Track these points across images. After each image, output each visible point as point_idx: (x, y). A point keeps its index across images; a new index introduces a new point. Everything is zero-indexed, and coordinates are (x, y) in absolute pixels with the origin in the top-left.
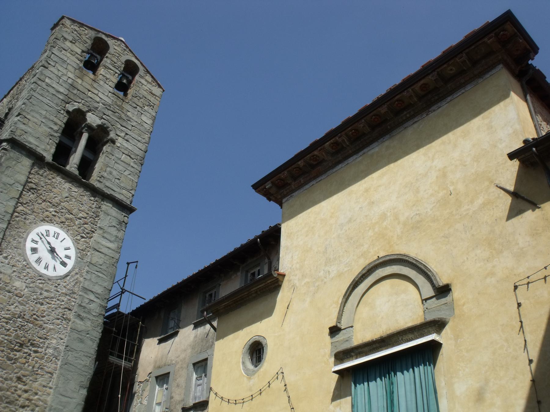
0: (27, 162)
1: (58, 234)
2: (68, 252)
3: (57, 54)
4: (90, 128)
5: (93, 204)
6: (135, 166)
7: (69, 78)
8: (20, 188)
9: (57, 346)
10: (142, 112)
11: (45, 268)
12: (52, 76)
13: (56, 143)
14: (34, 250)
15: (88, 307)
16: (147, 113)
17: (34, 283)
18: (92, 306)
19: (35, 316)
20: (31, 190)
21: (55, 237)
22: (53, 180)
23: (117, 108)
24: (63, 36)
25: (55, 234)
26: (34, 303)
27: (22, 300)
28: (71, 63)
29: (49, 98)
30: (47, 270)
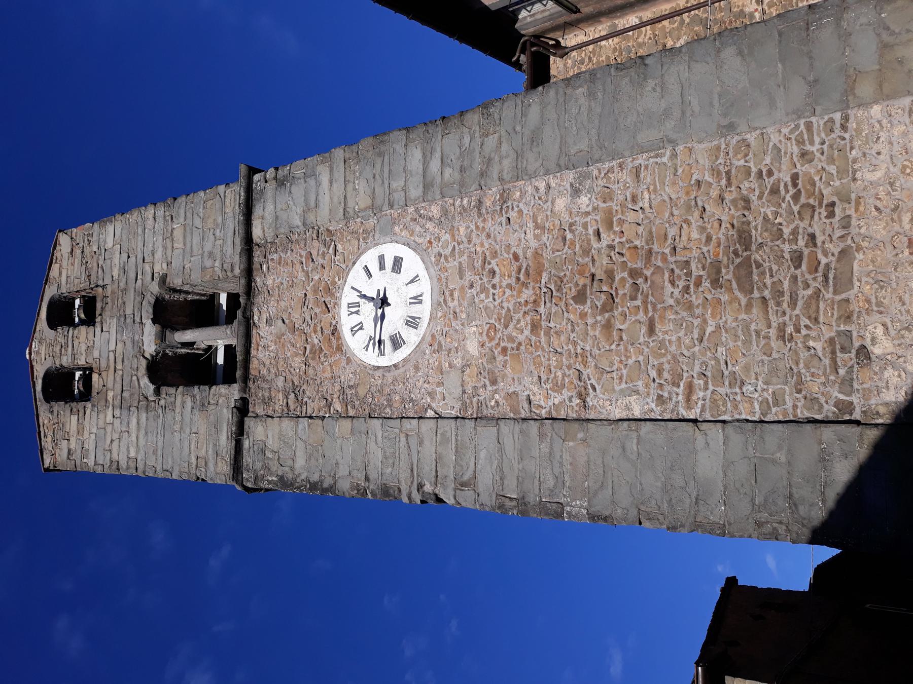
0: (256, 430)
1: (350, 305)
2: (374, 268)
3: (94, 457)
4: (161, 337)
5: (272, 259)
6: (182, 211)
7: (114, 417)
8: (304, 422)
9: (569, 189)
10: (103, 251)
11: (420, 302)
12: (123, 449)
13: (210, 389)
14: (397, 342)
15: (459, 164)
16: (101, 240)
17: (458, 311)
18: (453, 153)
19: (522, 276)
20: (300, 398)
21: (356, 309)
22: (267, 363)
23: (116, 303)
24: (68, 458)
25: (352, 313)
26: (496, 292)
27: (500, 323)
28: (94, 424)
29: (155, 439)
30: (421, 295)
